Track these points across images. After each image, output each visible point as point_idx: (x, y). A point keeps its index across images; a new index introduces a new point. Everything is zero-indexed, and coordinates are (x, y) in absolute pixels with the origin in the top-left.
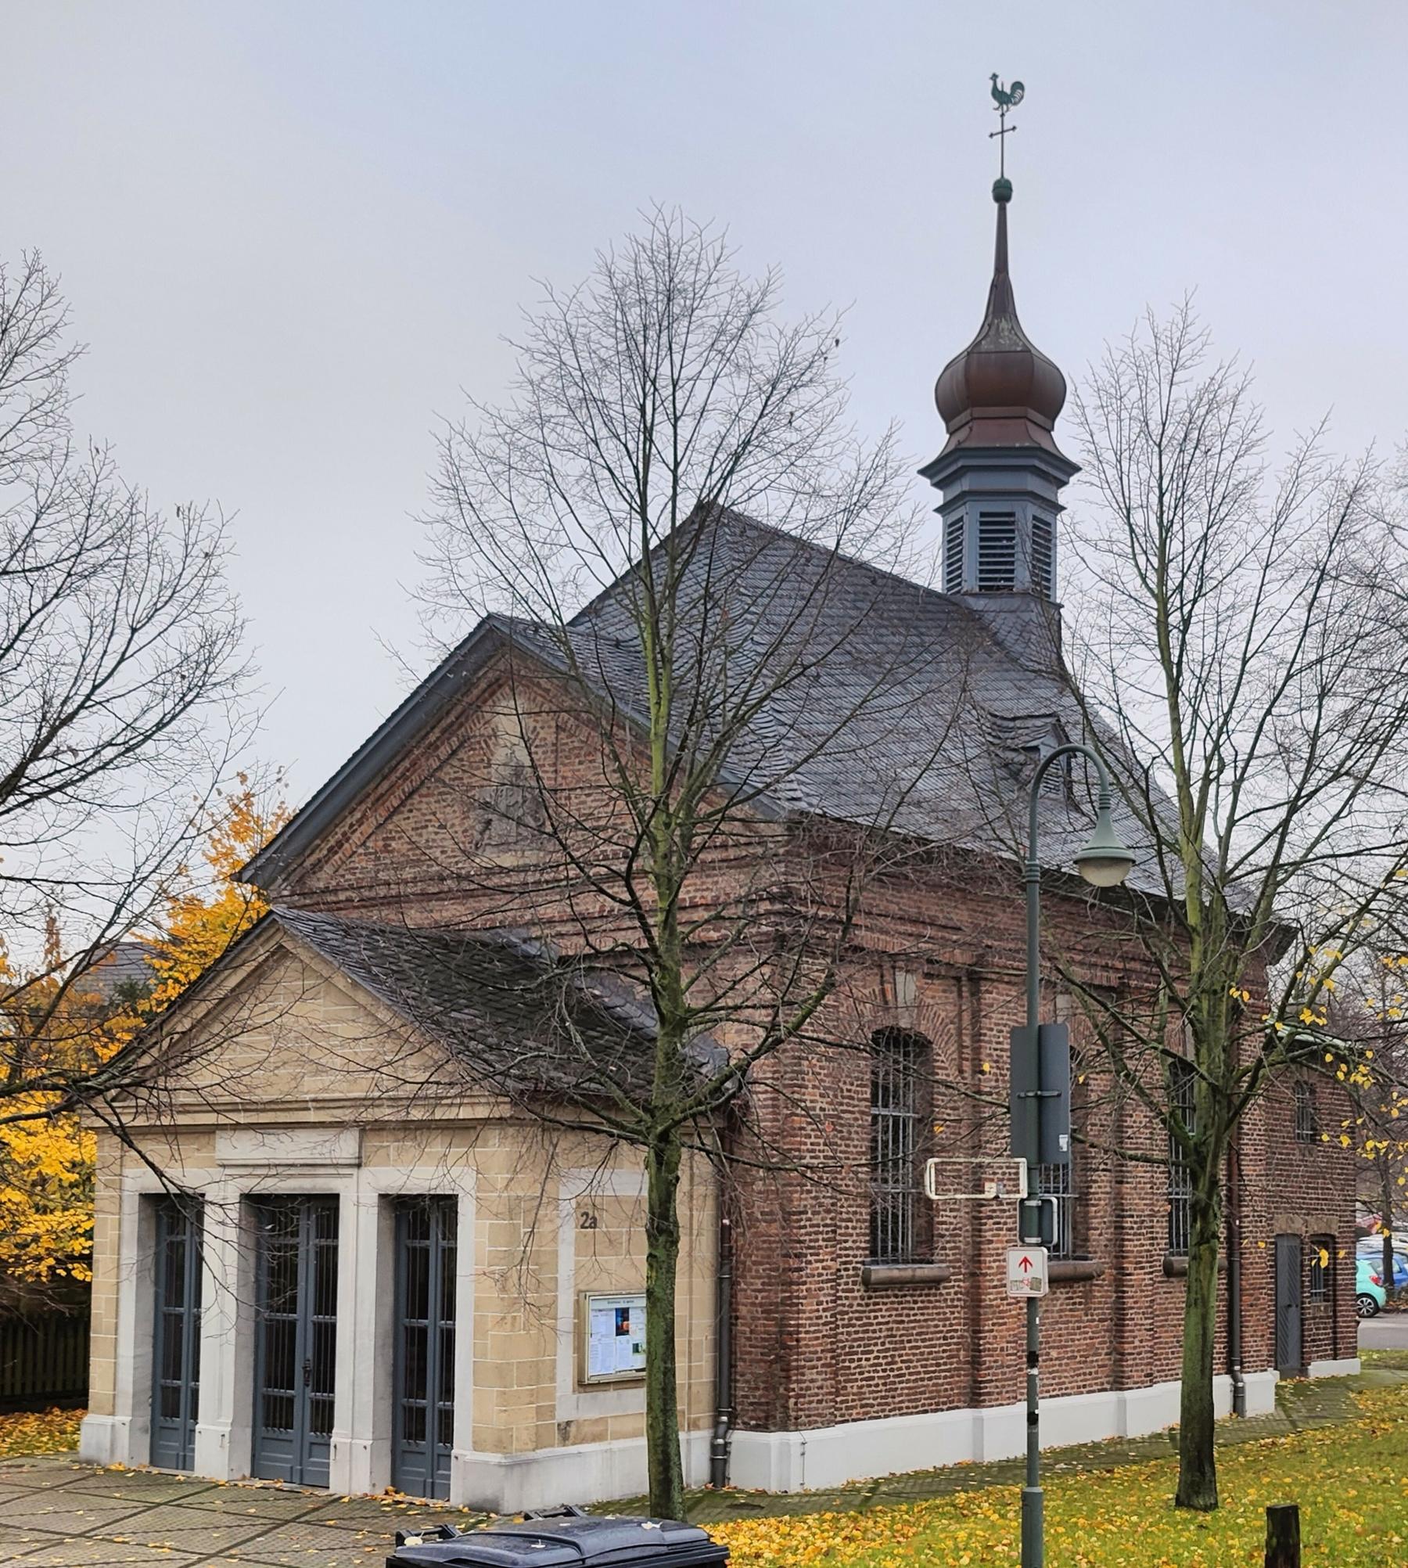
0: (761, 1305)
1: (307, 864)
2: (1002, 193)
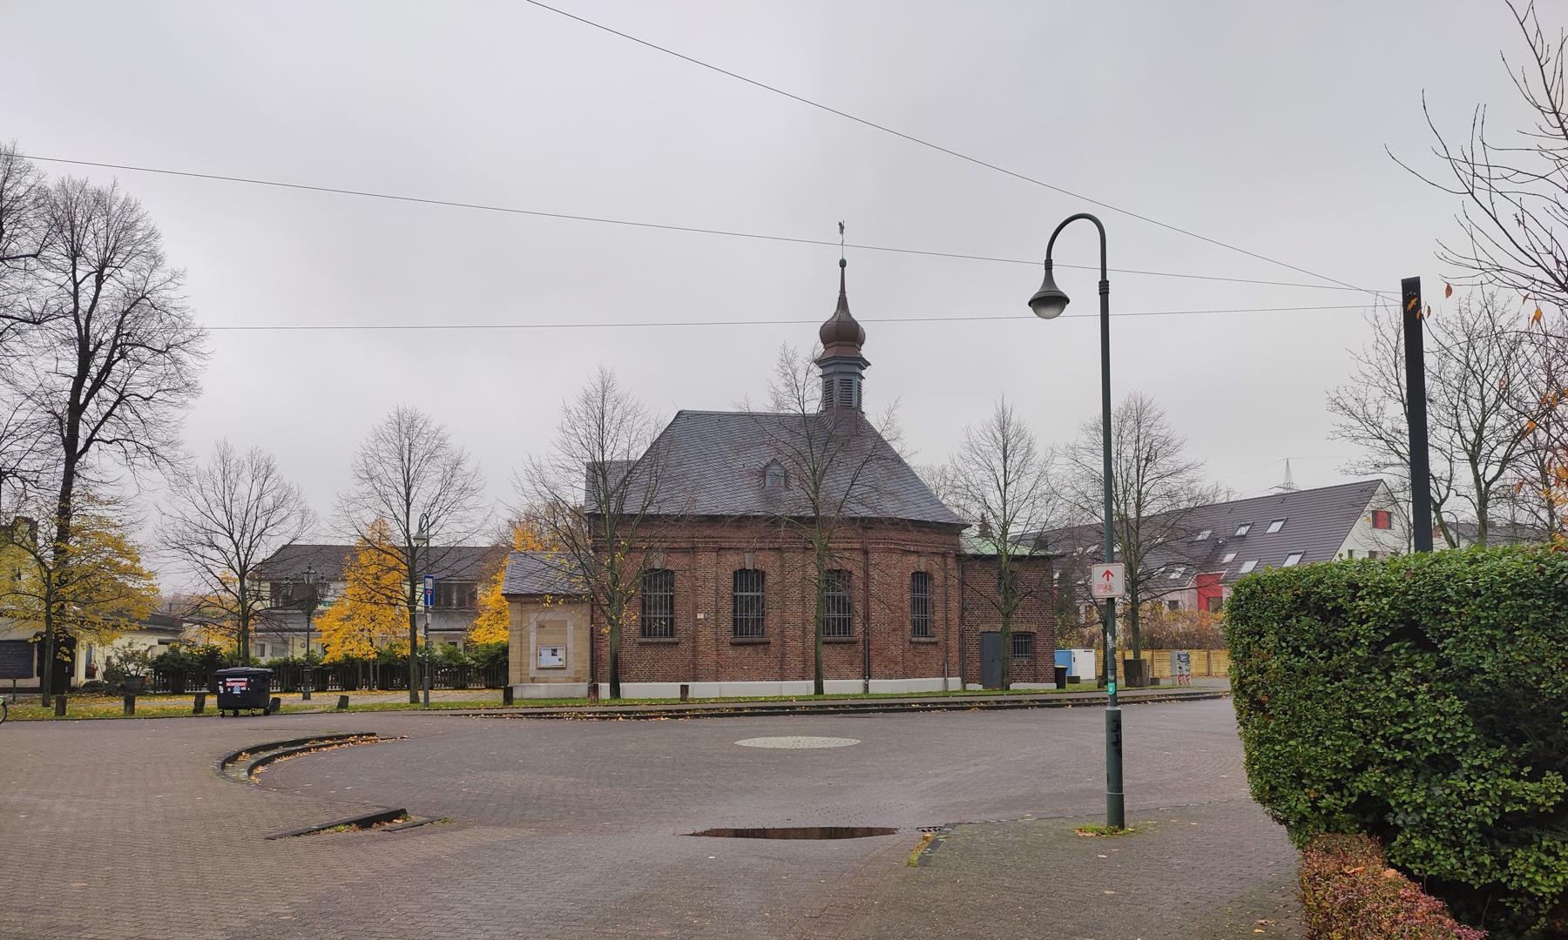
2: (843, 264)
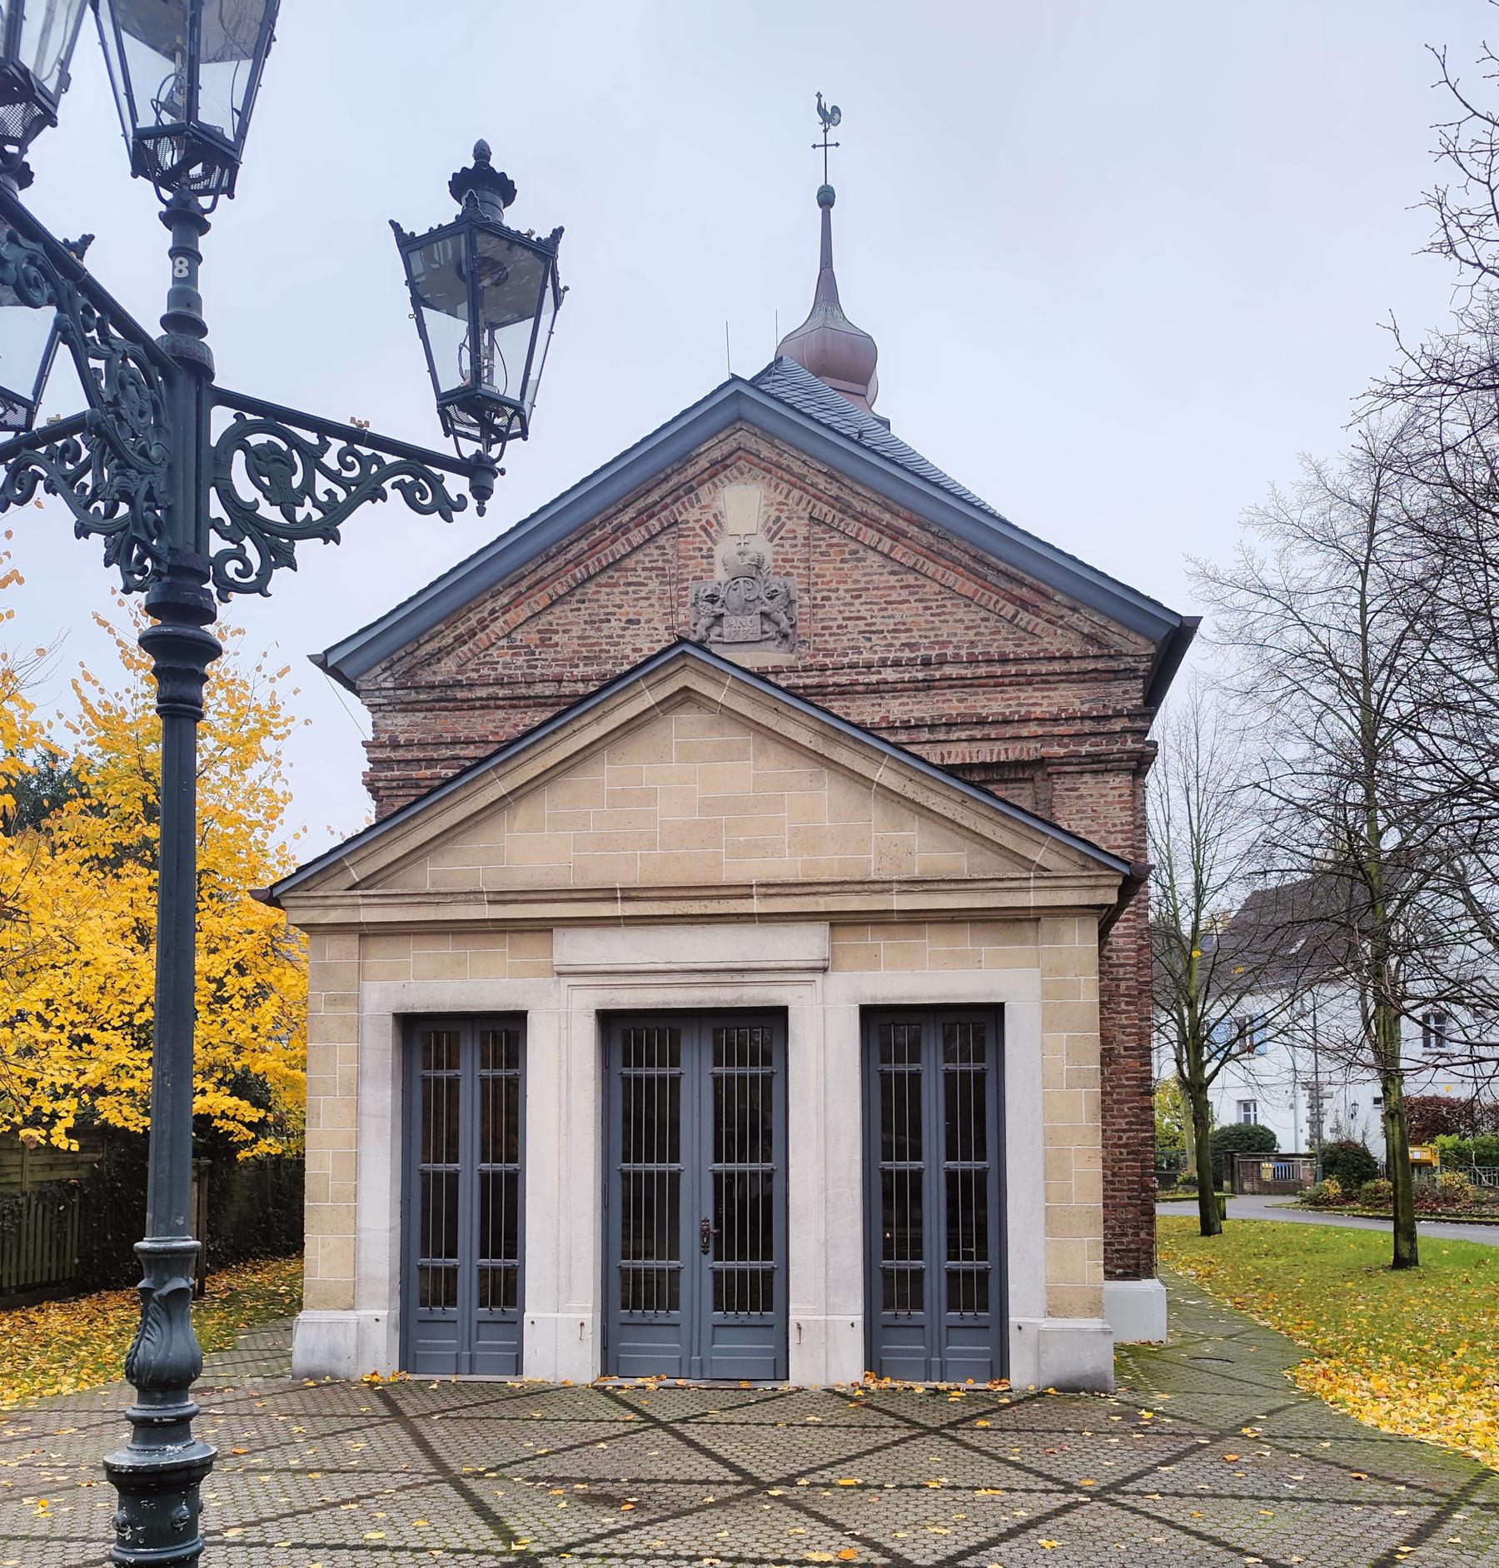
0: (1125, 1146)
1: (422, 652)
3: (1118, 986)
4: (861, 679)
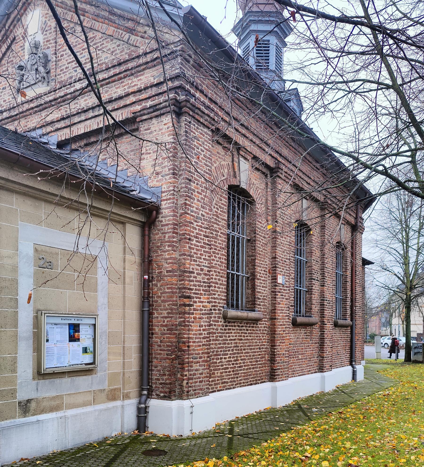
0: (166, 326)
3: (165, 237)
4: (68, 91)
